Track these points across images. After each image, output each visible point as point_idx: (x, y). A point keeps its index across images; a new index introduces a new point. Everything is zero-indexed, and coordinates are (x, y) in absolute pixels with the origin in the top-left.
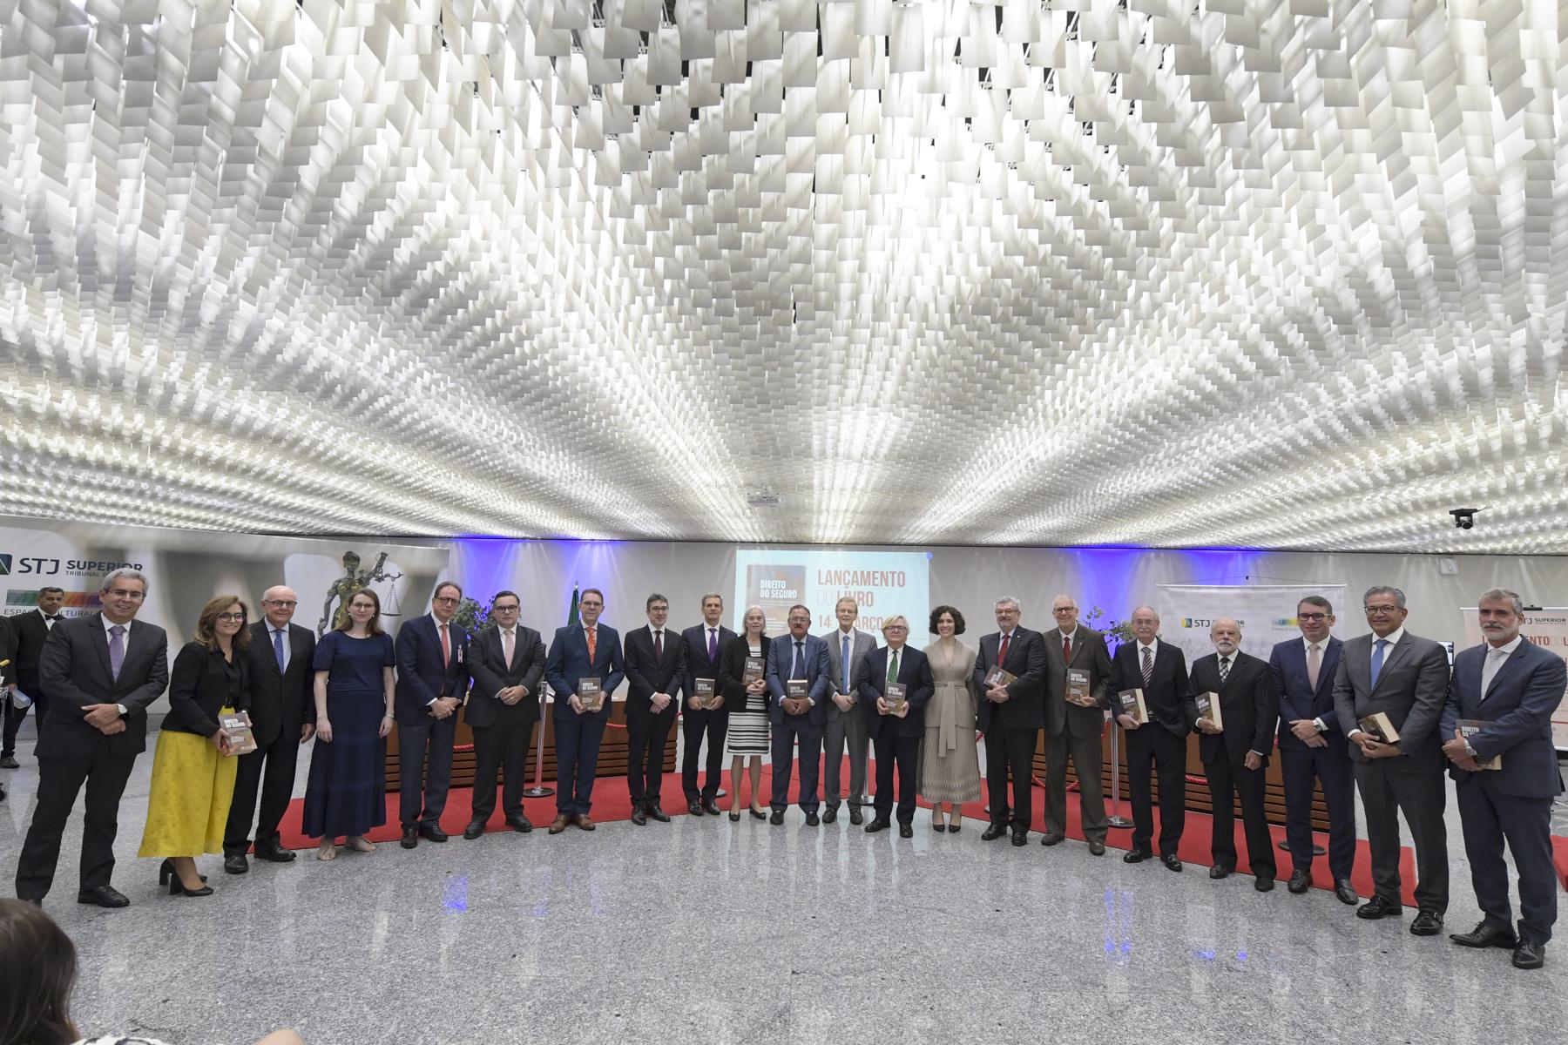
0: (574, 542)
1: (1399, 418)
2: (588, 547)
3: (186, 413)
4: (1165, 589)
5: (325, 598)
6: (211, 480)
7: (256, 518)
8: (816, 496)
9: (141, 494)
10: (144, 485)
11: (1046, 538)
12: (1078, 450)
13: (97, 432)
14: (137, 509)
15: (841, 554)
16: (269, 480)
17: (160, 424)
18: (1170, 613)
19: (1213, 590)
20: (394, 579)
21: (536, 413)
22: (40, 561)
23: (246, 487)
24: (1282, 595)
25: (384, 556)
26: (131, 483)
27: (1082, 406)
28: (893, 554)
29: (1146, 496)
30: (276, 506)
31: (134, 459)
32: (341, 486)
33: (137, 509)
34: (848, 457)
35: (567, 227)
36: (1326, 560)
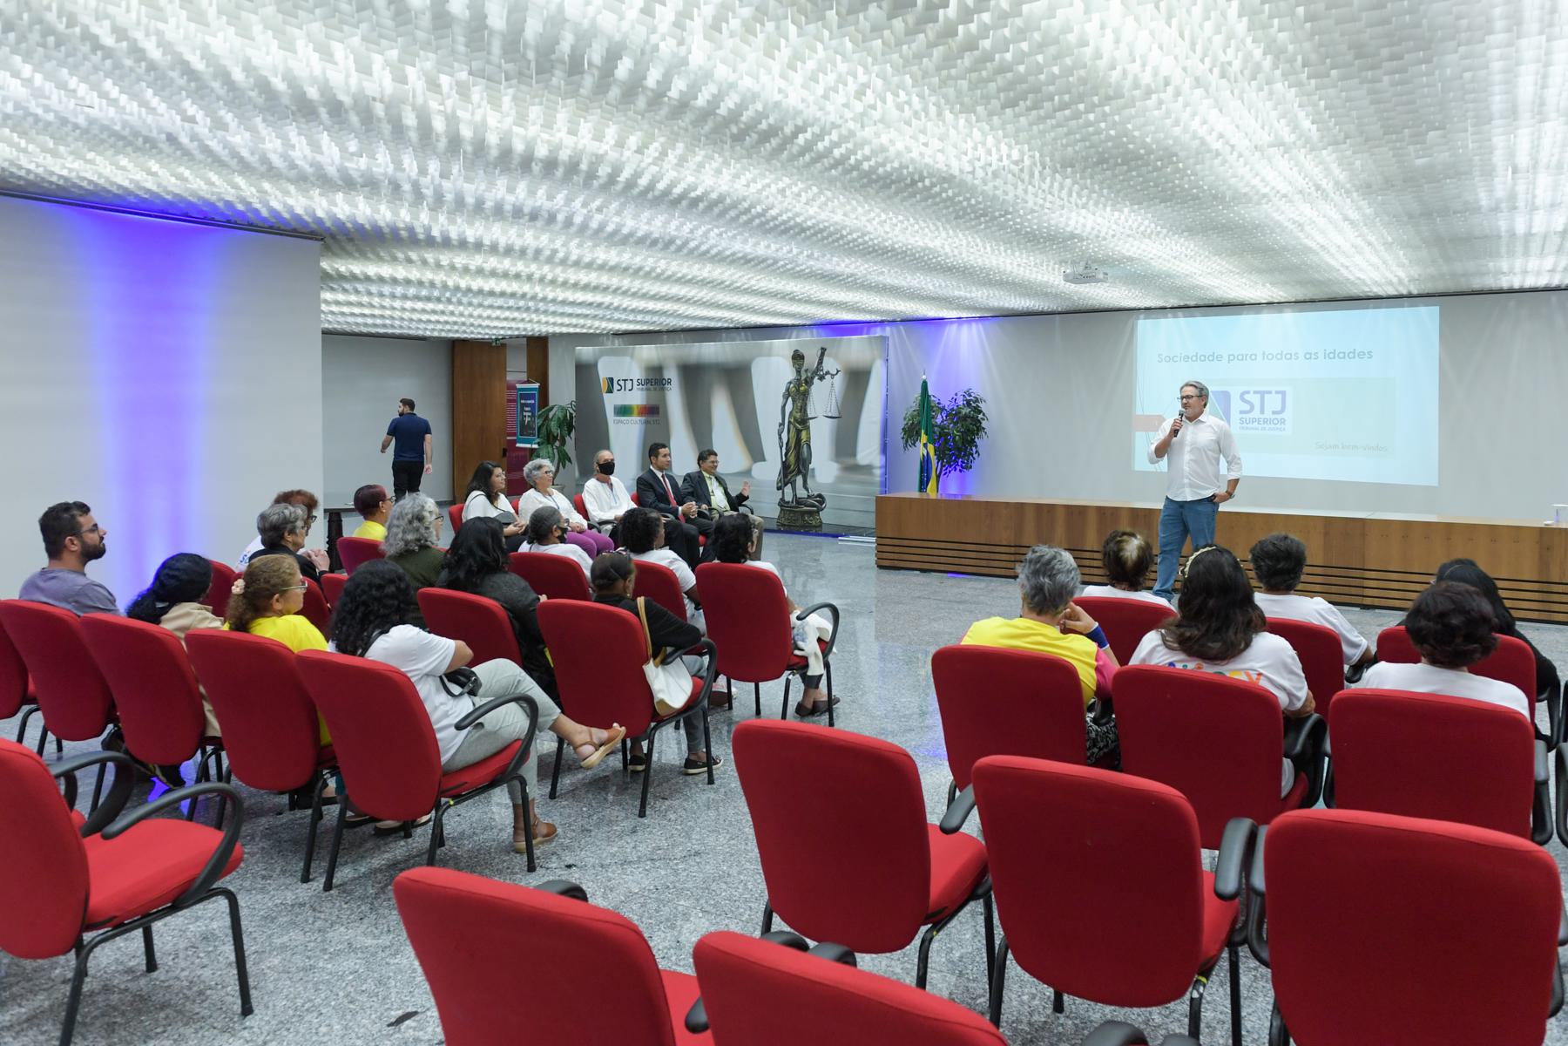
2: (954, 327)
3: (563, 262)
5: (781, 401)
6: (580, 296)
7: (618, 320)
9: (528, 309)
10: (531, 304)
13: (505, 275)
14: (523, 320)
15: (1289, 317)
16: (625, 293)
17: (546, 268)
22: (1262, 394)
23: (607, 299)
26: (521, 303)
28: (1370, 312)
30: (633, 311)
31: (526, 288)
33: (523, 320)
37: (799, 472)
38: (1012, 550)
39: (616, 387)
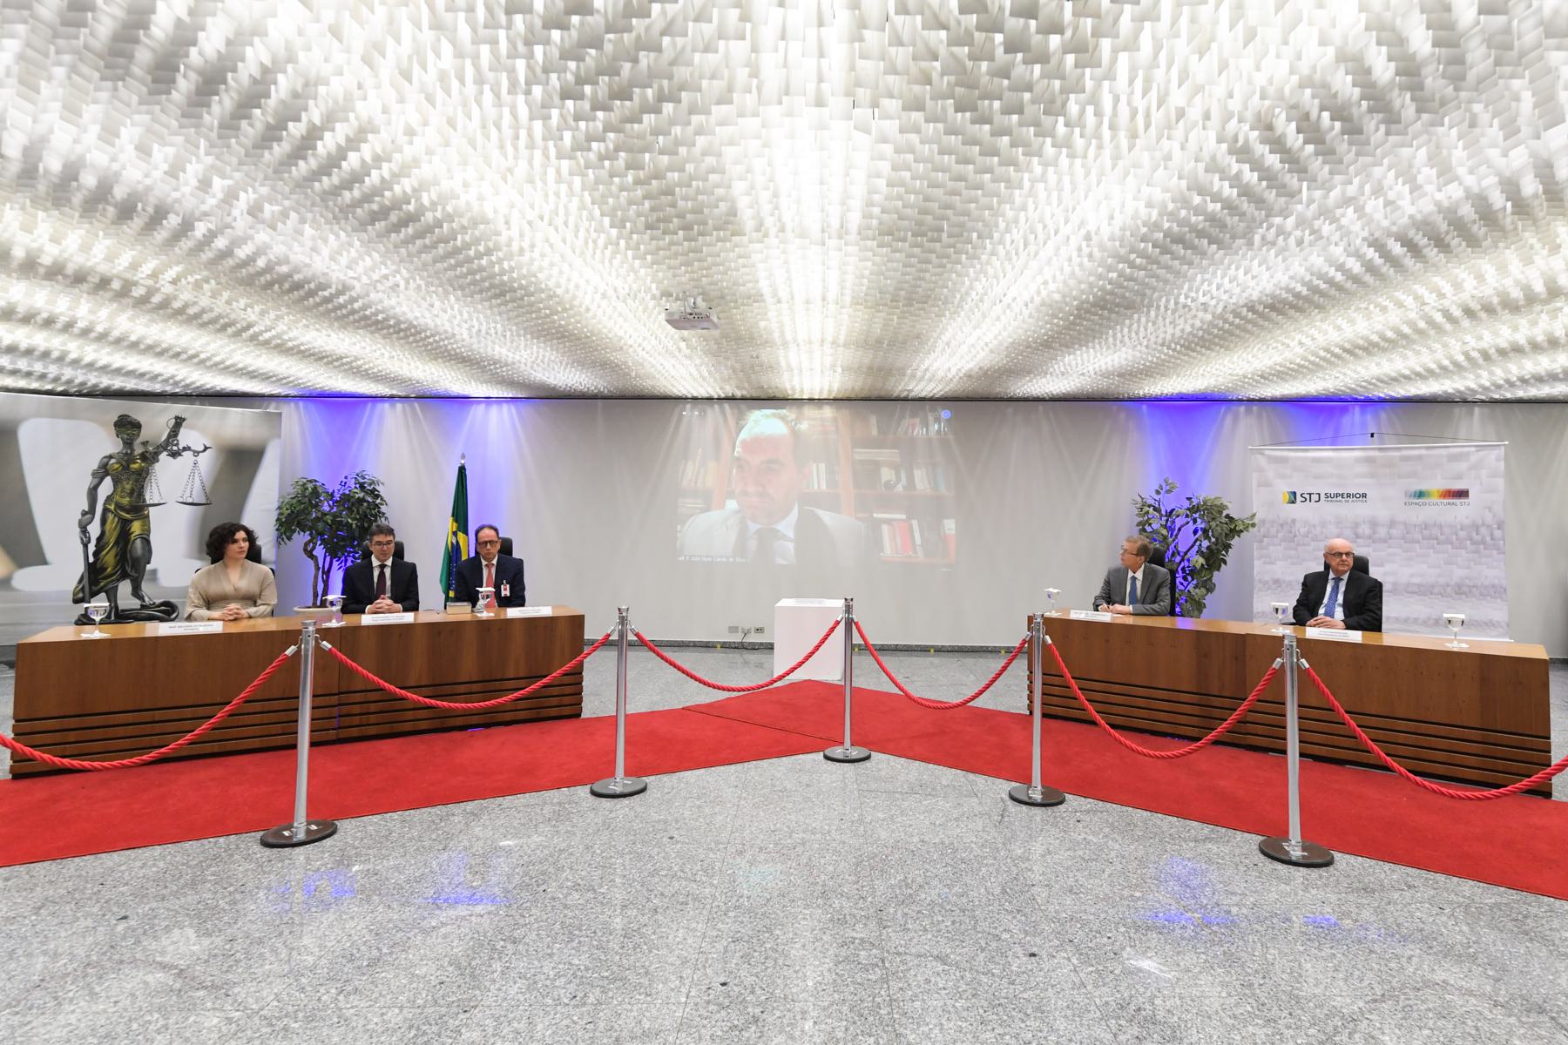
0: (464, 400)
1: (1441, 244)
2: (482, 407)
4: (1261, 452)
5: (88, 481)
8: (772, 314)
11: (1103, 385)
12: (1091, 286)
16: (102, 337)
18: (1267, 484)
19: (1325, 453)
20: (196, 453)
21: (406, 242)
24: (1420, 457)
25: (179, 422)
27: (1177, 98)
29: (1251, 309)
32: (292, 371)
34: (803, 234)
35: (502, 147)
36: (1471, 414)
37: (124, 576)
38: (334, 700)
39: (1299, 498)
